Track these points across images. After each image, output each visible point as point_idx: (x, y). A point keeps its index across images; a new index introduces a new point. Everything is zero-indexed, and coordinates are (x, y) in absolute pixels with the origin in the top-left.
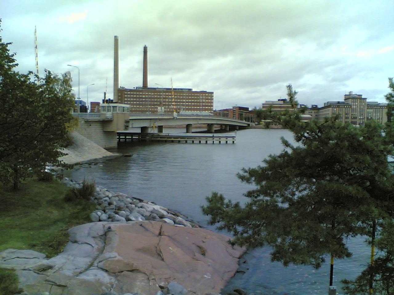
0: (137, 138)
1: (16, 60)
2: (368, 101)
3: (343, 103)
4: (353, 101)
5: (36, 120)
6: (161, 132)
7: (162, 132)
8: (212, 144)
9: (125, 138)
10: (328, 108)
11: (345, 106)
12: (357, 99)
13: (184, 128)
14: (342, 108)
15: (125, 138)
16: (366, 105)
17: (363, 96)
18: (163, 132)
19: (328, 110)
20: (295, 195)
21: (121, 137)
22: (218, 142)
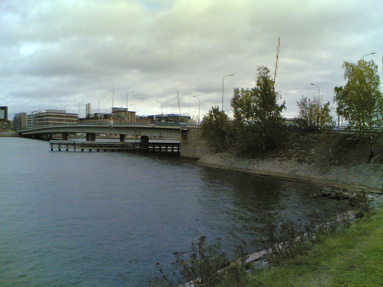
0: (152, 148)
1: (231, 106)
2: (137, 114)
3: (110, 115)
4: (125, 113)
5: (373, 146)
6: (93, 141)
7: (95, 141)
8: (81, 152)
9: (160, 149)
10: (88, 120)
11: (119, 118)
12: (125, 113)
13: (118, 139)
14: (117, 119)
15: (160, 149)
16: (135, 118)
17: (128, 109)
18: (96, 140)
19: (91, 121)
20: (246, 268)
21: (168, 148)
22: (65, 150)
